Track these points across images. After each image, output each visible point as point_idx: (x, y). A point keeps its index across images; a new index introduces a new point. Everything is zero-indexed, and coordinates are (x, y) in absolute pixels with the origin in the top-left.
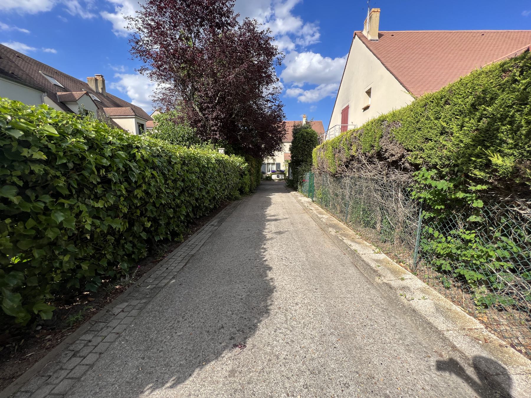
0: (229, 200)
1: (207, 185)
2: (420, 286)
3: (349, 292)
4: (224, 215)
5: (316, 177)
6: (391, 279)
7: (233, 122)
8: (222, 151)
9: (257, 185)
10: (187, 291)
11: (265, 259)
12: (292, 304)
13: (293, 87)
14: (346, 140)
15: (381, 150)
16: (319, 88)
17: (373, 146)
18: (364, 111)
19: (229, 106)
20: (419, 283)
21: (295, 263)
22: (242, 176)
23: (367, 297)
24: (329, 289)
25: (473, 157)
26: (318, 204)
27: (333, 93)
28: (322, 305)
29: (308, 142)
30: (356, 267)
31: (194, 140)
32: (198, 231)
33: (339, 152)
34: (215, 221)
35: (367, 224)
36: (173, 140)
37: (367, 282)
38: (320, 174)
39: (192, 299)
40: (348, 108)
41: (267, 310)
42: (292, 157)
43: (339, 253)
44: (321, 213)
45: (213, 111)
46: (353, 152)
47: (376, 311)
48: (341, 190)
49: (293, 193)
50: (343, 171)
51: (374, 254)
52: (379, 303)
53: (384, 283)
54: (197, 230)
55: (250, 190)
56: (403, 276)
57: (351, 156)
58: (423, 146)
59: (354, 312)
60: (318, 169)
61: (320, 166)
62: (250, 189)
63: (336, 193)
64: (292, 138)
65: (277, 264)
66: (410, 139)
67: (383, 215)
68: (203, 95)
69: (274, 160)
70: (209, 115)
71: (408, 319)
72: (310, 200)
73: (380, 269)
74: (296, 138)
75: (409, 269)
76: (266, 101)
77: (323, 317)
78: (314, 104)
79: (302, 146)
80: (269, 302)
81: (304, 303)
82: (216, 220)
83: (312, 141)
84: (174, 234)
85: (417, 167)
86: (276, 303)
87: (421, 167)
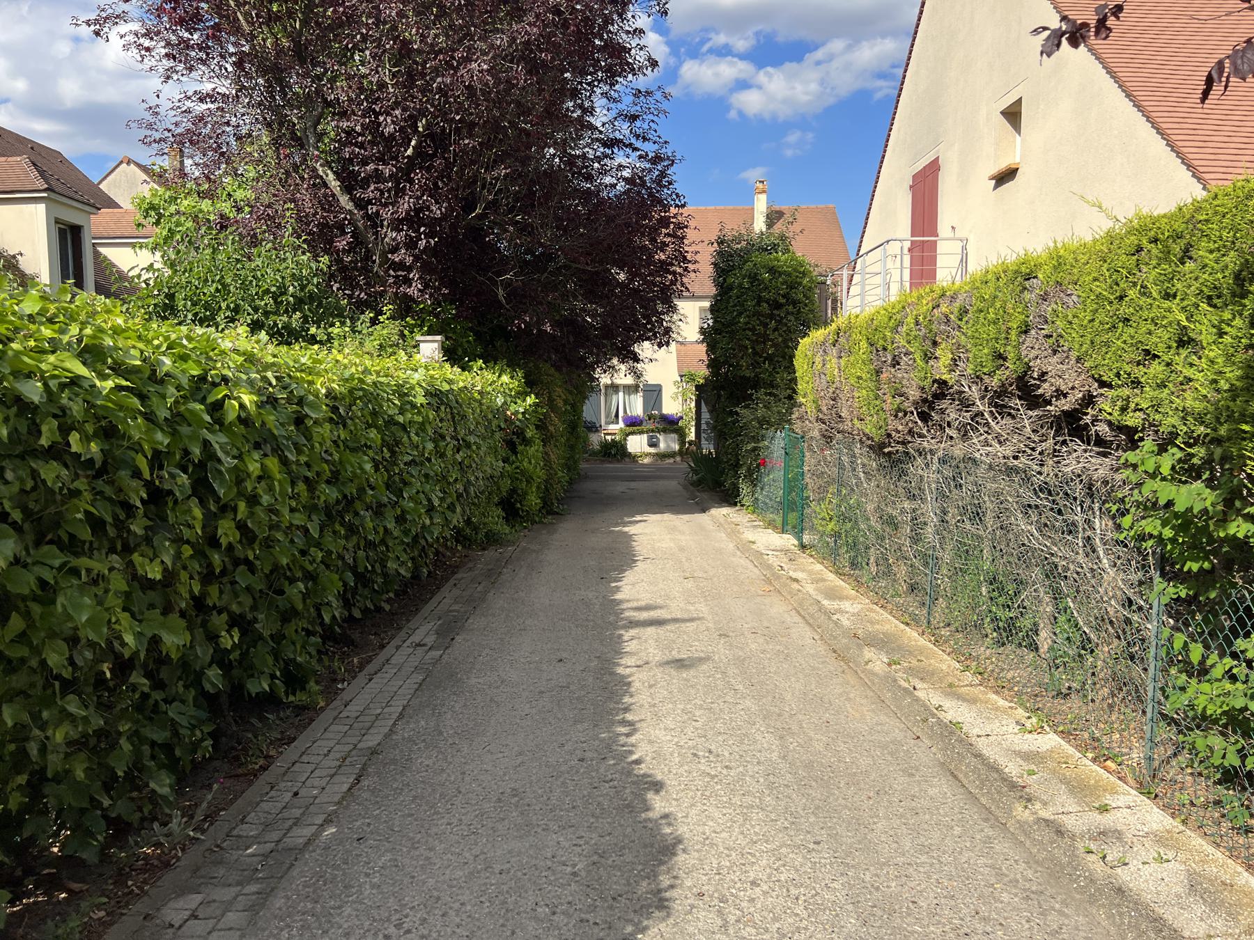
0: (464, 547)
1: (401, 491)
2: (1155, 827)
3: (925, 849)
4: (456, 607)
5: (810, 449)
6: (1065, 810)
7: (476, 233)
8: (430, 348)
9: (571, 482)
10: (388, 856)
11: (634, 757)
12: (739, 885)
13: (711, 51)
14: (917, 323)
15: (1026, 372)
16: (819, 54)
17: (1001, 357)
18: (996, 187)
19: (462, 170)
20: (1156, 818)
21: (741, 769)
22: (511, 446)
23: (981, 861)
24: (860, 842)
25: (1246, 423)
26: (822, 559)
27: (882, 76)
28: (835, 885)
29: (779, 306)
30: (955, 777)
31: (320, 305)
32: (370, 668)
33: (896, 363)
34: (423, 630)
35: (1008, 632)
36: (237, 306)
37: (986, 820)
38: (828, 438)
39: (413, 877)
40: (933, 168)
41: (662, 900)
42: (713, 365)
43: (898, 735)
44: (832, 594)
45: (400, 192)
46: (941, 369)
47: (1005, 897)
48: (907, 505)
49: (722, 513)
50: (910, 432)
51: (1020, 736)
52: (1019, 876)
53: (1039, 820)
54: (362, 667)
55: (545, 503)
56: (1108, 800)
57: (935, 381)
58: (1138, 372)
59: (935, 901)
60: (818, 419)
61: (824, 409)
62: (544, 499)
63: (891, 517)
64: (712, 290)
65: (681, 770)
66: (1104, 349)
67: (1057, 596)
68: (358, 128)
69: (638, 376)
70: (386, 205)
71: (1102, 915)
72: (789, 541)
73: (1033, 783)
74: (731, 288)
75: (1130, 780)
76: (605, 145)
77: (837, 915)
78: (801, 122)
79: (755, 322)
80: (665, 881)
81: (778, 881)
82: (429, 626)
83: (794, 303)
84: (295, 679)
85: (1131, 438)
86: (688, 883)
87: (1142, 439)
